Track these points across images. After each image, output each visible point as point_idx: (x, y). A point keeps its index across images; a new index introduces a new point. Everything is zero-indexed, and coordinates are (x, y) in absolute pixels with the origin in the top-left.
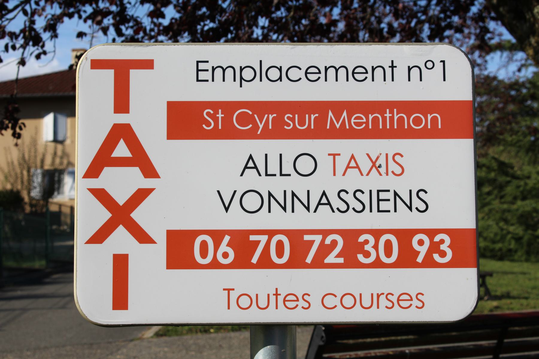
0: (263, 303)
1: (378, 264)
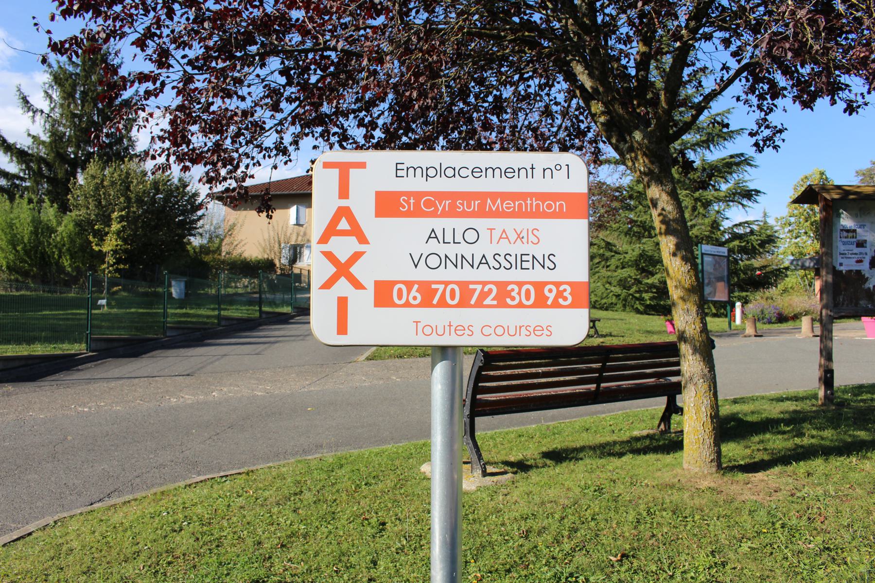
0: (440, 332)
1: (520, 305)
